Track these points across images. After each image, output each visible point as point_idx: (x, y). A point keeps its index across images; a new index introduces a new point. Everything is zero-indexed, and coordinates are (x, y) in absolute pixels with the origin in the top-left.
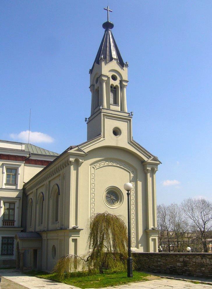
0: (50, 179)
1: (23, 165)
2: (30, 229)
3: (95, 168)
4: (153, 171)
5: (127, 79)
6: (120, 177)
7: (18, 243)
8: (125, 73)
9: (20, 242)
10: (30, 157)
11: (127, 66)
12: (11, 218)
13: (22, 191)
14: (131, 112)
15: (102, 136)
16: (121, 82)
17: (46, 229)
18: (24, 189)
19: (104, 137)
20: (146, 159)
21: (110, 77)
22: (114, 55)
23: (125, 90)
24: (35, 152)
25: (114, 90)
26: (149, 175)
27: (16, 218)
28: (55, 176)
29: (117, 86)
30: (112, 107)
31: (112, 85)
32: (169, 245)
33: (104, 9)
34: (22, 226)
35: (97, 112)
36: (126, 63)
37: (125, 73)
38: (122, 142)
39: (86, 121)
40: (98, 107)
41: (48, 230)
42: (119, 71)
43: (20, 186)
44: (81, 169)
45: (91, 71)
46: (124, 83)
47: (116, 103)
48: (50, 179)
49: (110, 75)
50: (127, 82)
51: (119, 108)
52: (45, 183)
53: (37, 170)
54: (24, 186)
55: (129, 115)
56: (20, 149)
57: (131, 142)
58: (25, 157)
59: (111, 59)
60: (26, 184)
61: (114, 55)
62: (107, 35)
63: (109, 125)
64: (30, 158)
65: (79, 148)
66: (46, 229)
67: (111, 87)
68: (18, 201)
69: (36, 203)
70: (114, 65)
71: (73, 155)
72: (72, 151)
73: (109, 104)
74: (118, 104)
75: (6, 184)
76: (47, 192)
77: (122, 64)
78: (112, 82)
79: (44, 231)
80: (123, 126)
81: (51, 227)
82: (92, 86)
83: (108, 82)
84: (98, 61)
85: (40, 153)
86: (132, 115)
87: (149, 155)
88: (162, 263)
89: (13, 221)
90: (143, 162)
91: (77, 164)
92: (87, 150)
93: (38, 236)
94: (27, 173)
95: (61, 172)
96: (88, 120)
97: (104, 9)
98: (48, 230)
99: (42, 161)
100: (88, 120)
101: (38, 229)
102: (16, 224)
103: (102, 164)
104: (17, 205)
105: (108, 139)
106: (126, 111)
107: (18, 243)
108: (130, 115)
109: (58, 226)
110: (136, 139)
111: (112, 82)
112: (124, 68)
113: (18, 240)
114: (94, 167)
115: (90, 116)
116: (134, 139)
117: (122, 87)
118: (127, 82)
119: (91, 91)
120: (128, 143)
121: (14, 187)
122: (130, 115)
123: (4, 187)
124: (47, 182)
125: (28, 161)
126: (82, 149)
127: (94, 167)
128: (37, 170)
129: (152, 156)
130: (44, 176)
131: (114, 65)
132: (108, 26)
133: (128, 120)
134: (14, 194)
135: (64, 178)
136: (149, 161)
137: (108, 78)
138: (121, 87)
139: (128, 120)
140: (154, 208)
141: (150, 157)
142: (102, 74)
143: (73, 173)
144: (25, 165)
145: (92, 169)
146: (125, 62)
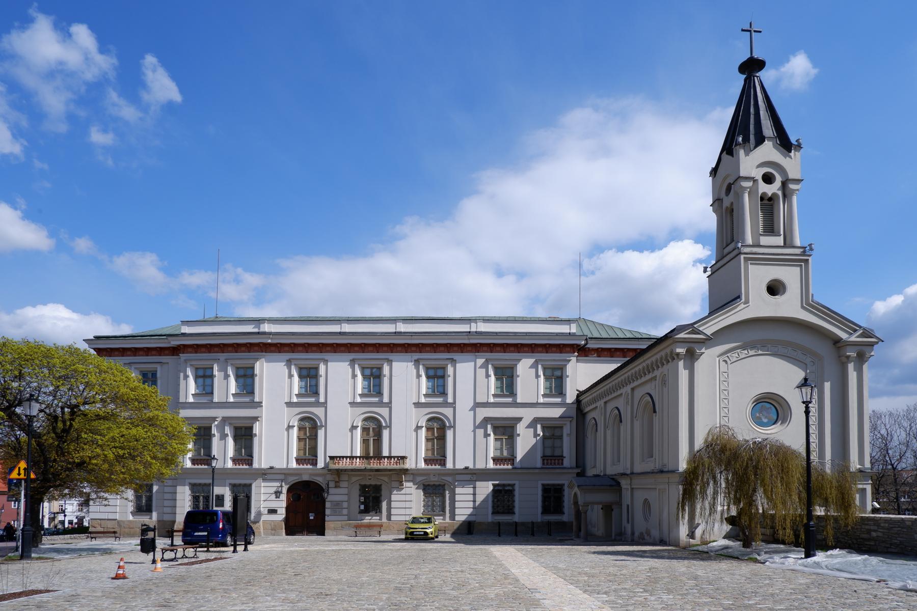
0: (633, 385)
1: (574, 359)
2: (590, 472)
3: (729, 362)
4: (861, 358)
5: (798, 177)
6: (781, 376)
7: (575, 494)
8: (793, 164)
9: (579, 493)
10: (586, 344)
11: (799, 146)
12: (557, 453)
13: (575, 406)
14: (810, 245)
15: (743, 300)
16: (784, 184)
17: (629, 472)
18: (578, 401)
19: (747, 302)
20: (843, 336)
21: (759, 178)
22: (768, 129)
23: (795, 199)
24: (596, 335)
25: (768, 203)
26: (851, 366)
27: (566, 453)
28: (644, 379)
29: (774, 194)
30: (765, 240)
31: (764, 194)
32: (897, 498)
33: (743, 30)
34: (577, 467)
35: (730, 253)
36: (797, 141)
37: (793, 164)
38: (788, 306)
39: (705, 271)
40: (732, 246)
41: (632, 473)
42: (776, 161)
43: (571, 397)
44: (699, 365)
45: (714, 172)
46: (792, 186)
47: (770, 229)
48: (633, 385)
49: (758, 174)
50: (798, 181)
51: (780, 241)
52: (623, 391)
53: (604, 368)
54: (578, 396)
55: (804, 252)
56: (568, 331)
57: (808, 304)
58: (578, 345)
59: (760, 140)
60: (580, 394)
61: (768, 129)
62: (750, 87)
63: (757, 277)
64: (588, 346)
65: (692, 328)
66: (629, 472)
67: (762, 199)
68: (568, 424)
69: (606, 427)
70: (768, 151)
71: (684, 341)
72: (682, 335)
73: (756, 236)
74: (779, 232)
75: (544, 396)
76: (629, 408)
77: (785, 144)
78: (764, 188)
79: (623, 475)
80: (790, 275)
81: (638, 469)
82: (717, 203)
83: (752, 192)
84: (728, 148)
85: (605, 335)
86: (811, 249)
87: (851, 326)
88: (880, 534)
89: (561, 457)
90: (836, 342)
91: (692, 356)
92: (710, 329)
93: (613, 483)
94: (582, 374)
95: (657, 373)
96: (709, 269)
97: (743, 30)
98: (632, 473)
99: (609, 350)
100: (709, 269)
101: (610, 471)
102: (567, 463)
103: (734, 356)
104: (566, 430)
105: (758, 304)
106: (798, 242)
107: (575, 494)
108: (806, 251)
109: (649, 466)
110: (820, 296)
111: (764, 188)
112: (792, 154)
113: (576, 489)
114: (726, 359)
115: (714, 262)
116: (816, 299)
117: (786, 193)
118: (798, 181)
119: (714, 211)
120: (803, 307)
121: (558, 400)
122: (806, 251)
123: (541, 400)
124: (628, 389)
125: (583, 351)
126: (701, 329)
127: (726, 359)
128: (604, 368)
129: (860, 327)
130: (623, 377)
131: (768, 151)
132: (751, 67)
133: (802, 260)
134: (557, 413)
135: (664, 382)
136: (853, 338)
137: (755, 181)
138: (785, 196)
139: (802, 260)
140: (7, 599)
141: (855, 331)
142: (740, 178)
143: (683, 374)
144: (578, 361)
145: (723, 364)
146: (793, 140)
